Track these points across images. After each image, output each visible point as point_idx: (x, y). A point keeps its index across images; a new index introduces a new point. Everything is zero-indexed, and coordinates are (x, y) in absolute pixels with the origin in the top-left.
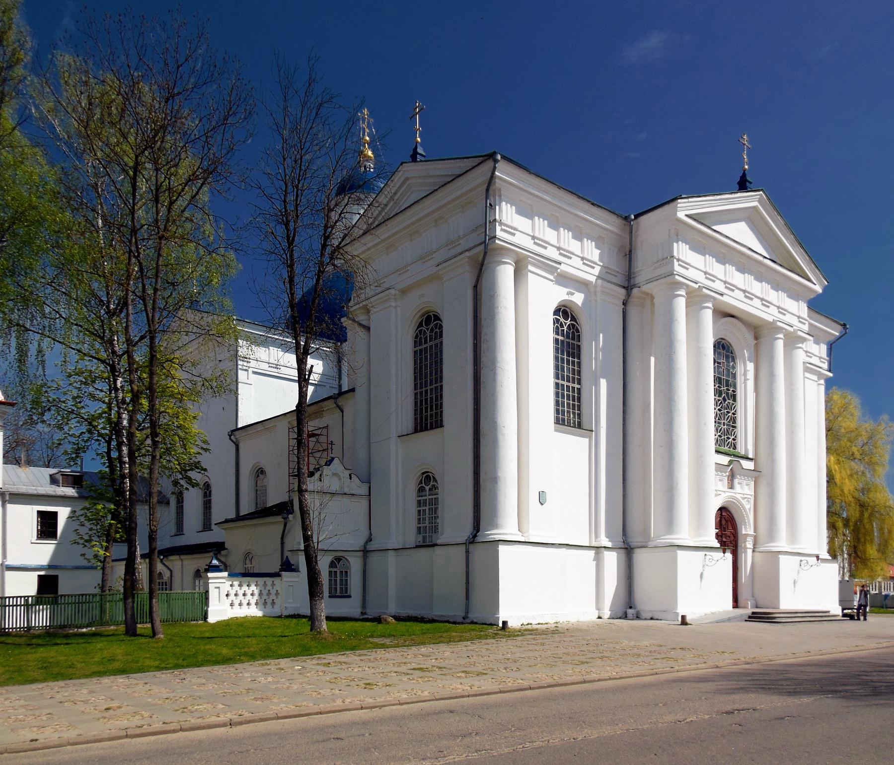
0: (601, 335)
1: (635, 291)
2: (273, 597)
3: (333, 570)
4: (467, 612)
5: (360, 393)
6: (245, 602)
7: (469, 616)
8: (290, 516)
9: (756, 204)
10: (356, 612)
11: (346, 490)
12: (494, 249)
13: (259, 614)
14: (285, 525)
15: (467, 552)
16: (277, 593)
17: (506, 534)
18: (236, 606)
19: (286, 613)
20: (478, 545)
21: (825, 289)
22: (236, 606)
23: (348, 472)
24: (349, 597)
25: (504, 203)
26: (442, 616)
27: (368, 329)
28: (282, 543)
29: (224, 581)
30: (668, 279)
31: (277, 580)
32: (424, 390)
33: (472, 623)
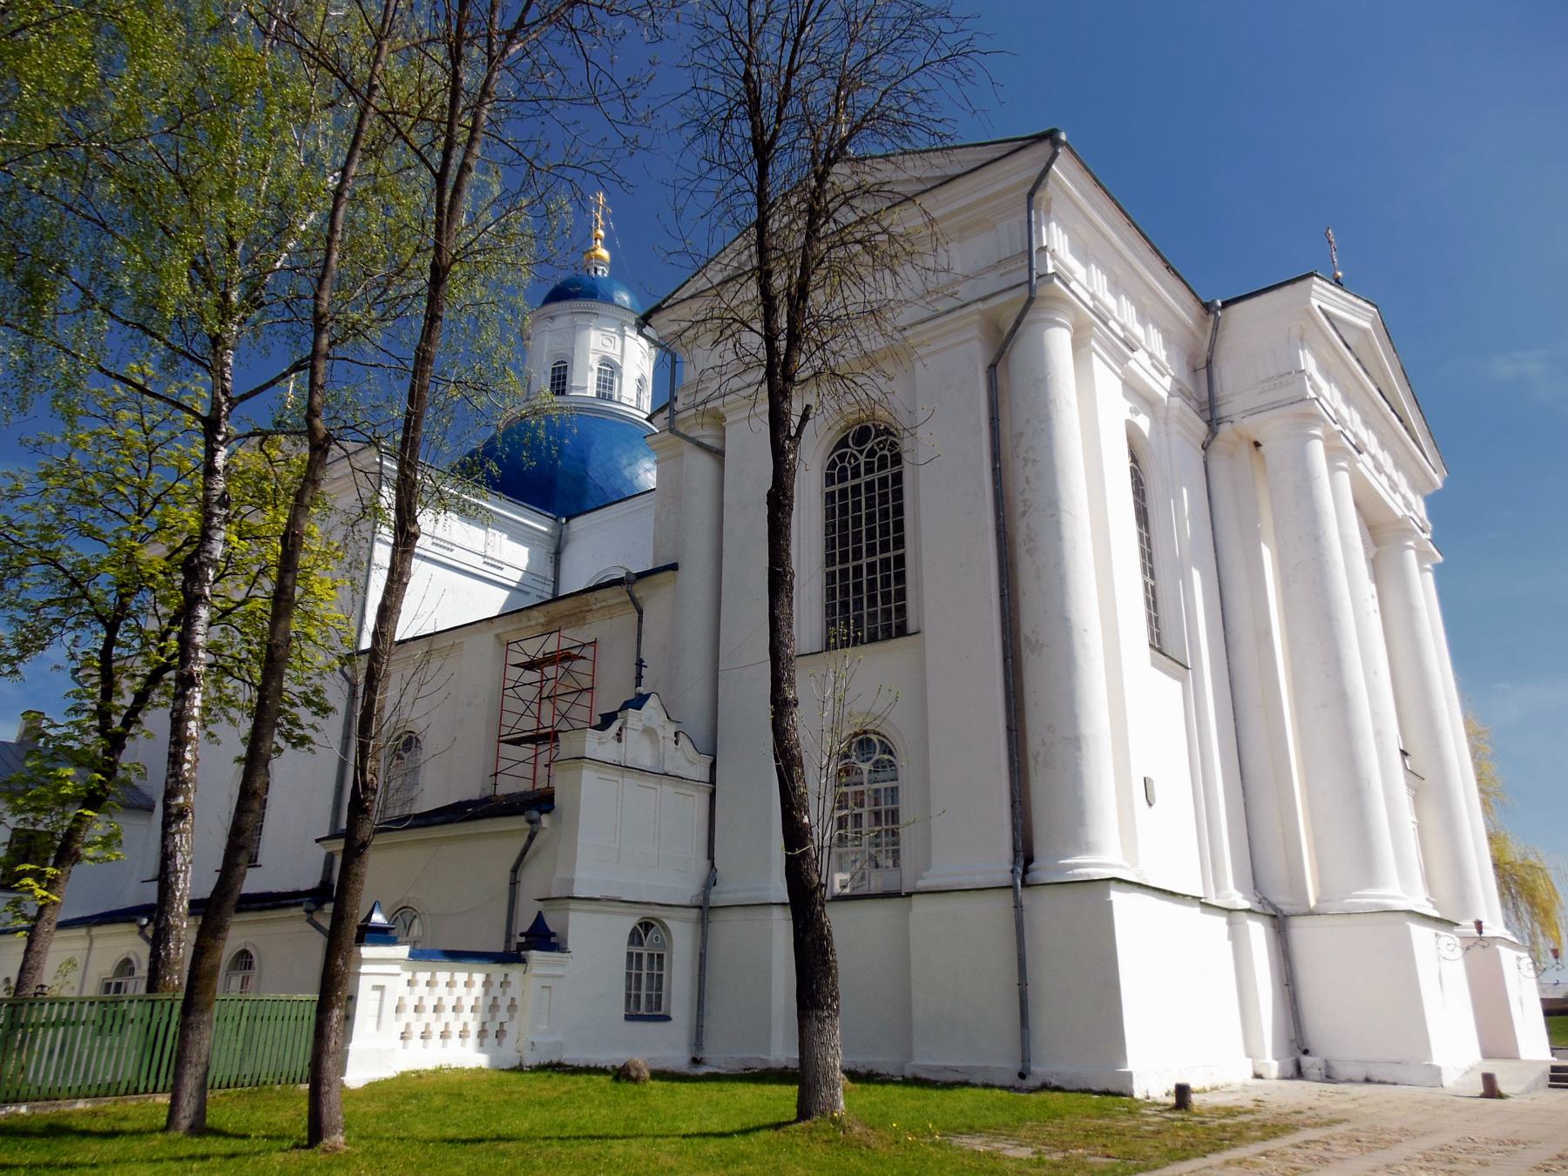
0: (1185, 491)
1: (1224, 429)
2: (503, 1015)
3: (636, 950)
4: (1025, 1058)
5: (696, 575)
6: (436, 1029)
7: (1033, 1068)
8: (545, 820)
9: (1367, 325)
10: (678, 1059)
11: (669, 768)
12: (1043, 298)
13: (480, 1060)
14: (531, 838)
15: (1018, 906)
16: (512, 1007)
17: (1112, 866)
18: (415, 1041)
19: (531, 1060)
20: (1045, 893)
21: (1446, 482)
22: (415, 1041)
23: (672, 729)
24: (667, 1018)
25: (1053, 225)
26: (946, 1068)
27: (718, 454)
28: (514, 883)
29: (396, 969)
30: (1298, 408)
31: (515, 971)
32: (851, 565)
33: (1045, 1087)
